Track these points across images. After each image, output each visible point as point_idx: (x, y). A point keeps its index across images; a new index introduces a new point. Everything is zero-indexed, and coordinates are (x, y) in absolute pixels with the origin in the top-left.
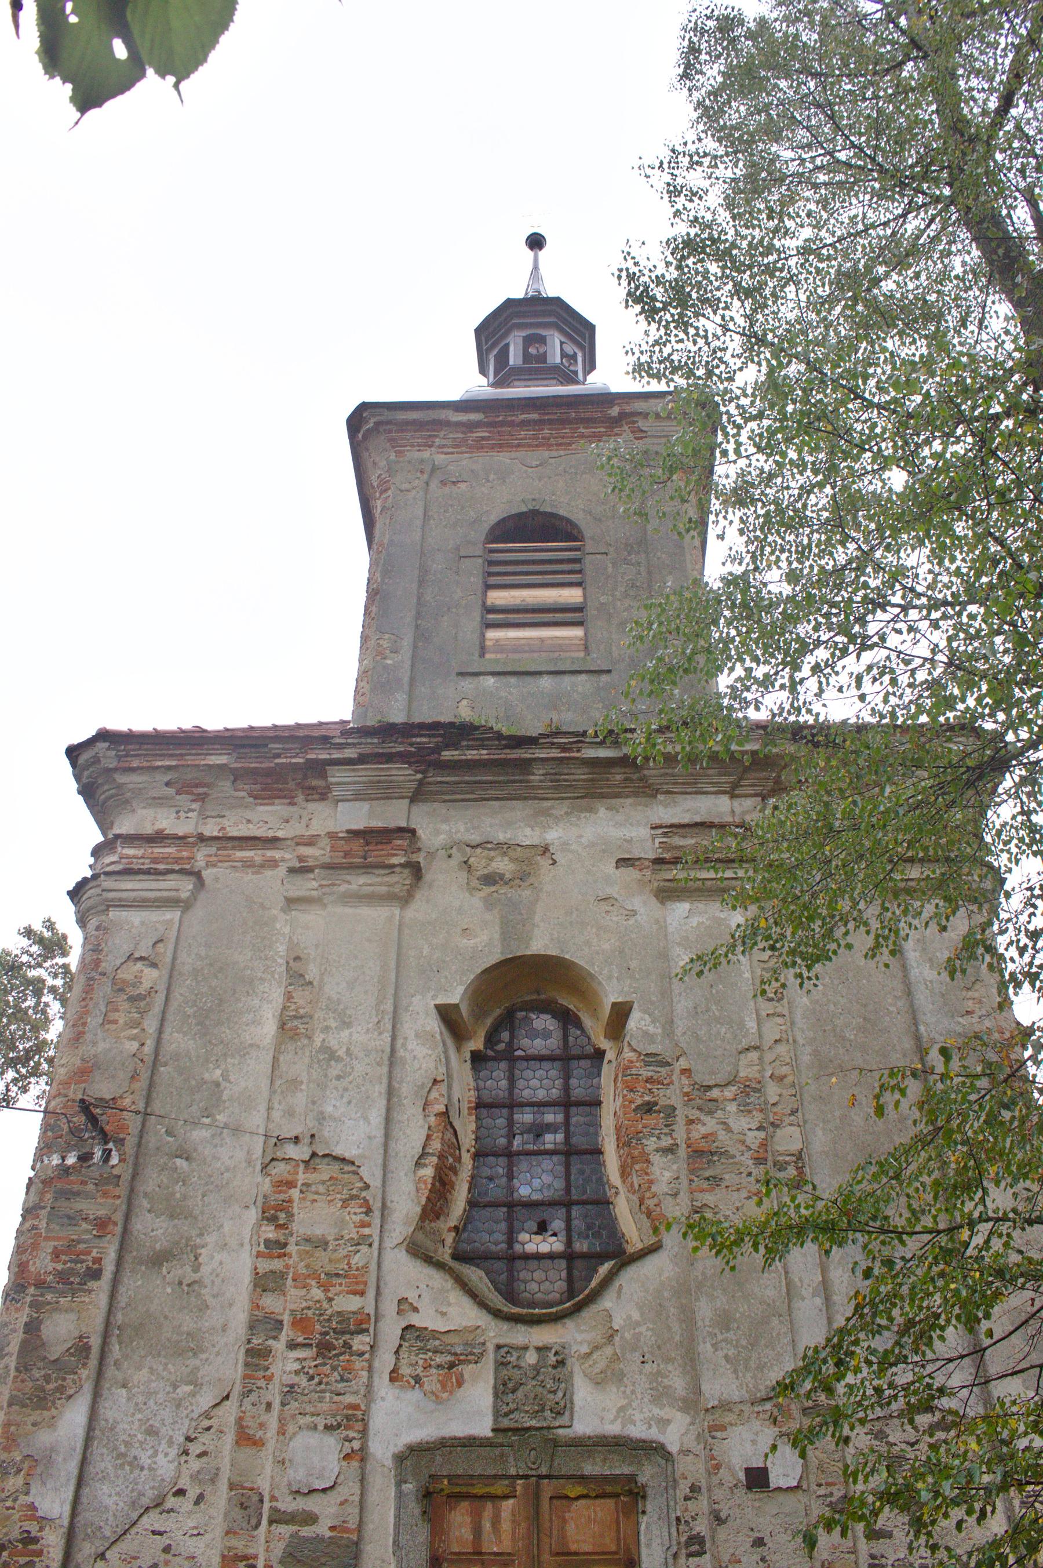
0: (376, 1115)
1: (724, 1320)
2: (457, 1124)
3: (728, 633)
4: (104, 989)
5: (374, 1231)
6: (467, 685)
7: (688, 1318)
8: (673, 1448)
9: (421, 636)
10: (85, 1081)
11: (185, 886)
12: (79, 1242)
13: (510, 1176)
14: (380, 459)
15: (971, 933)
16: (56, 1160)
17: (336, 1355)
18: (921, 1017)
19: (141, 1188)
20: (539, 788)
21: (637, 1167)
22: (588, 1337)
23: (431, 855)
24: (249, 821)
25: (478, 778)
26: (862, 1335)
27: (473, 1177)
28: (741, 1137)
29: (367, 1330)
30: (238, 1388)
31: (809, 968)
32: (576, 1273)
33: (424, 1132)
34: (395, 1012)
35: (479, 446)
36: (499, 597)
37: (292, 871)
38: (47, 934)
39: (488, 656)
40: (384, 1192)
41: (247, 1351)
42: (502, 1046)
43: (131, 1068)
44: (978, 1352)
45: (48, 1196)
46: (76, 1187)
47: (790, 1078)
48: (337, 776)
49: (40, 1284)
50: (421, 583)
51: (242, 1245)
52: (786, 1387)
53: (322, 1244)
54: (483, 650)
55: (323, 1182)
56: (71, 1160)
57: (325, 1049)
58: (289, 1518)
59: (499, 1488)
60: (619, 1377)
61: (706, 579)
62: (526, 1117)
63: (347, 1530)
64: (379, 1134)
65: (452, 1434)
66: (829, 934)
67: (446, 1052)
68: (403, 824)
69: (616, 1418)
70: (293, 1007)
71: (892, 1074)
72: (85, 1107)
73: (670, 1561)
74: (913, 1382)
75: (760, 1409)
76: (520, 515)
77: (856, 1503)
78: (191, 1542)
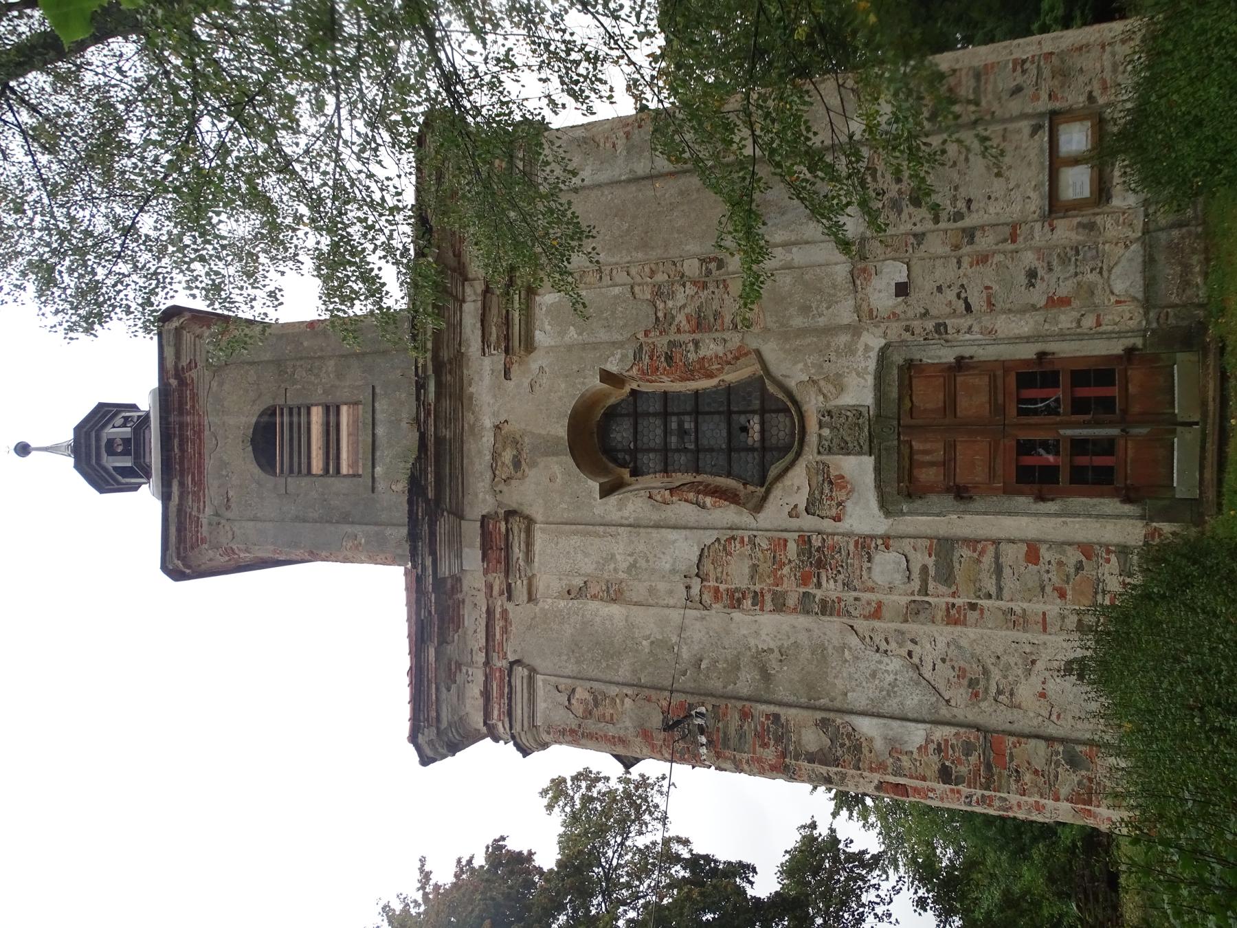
0: (672, 535)
1: (805, 309)
4: (591, 726)
5: (746, 534)
6: (381, 486)
7: (802, 332)
8: (883, 342)
9: (346, 519)
11: (520, 672)
12: (756, 730)
14: (207, 555)
16: (703, 750)
18: (616, 178)
20: (455, 432)
21: (707, 365)
24: (475, 632)
30: (845, 620)
32: (773, 408)
33: (683, 503)
35: (199, 484)
36: (317, 465)
38: (550, 794)
40: (722, 529)
41: (822, 614)
42: (627, 457)
43: (642, 702)
46: (721, 735)
47: (652, 266)
48: (444, 570)
50: (305, 521)
53: (754, 567)
55: (715, 568)
56: (703, 740)
59: (906, 451)
60: (839, 376)
63: (931, 546)
64: (684, 532)
67: (631, 491)
68: (478, 524)
73: (949, 344)
76: (254, 450)
78: (939, 645)
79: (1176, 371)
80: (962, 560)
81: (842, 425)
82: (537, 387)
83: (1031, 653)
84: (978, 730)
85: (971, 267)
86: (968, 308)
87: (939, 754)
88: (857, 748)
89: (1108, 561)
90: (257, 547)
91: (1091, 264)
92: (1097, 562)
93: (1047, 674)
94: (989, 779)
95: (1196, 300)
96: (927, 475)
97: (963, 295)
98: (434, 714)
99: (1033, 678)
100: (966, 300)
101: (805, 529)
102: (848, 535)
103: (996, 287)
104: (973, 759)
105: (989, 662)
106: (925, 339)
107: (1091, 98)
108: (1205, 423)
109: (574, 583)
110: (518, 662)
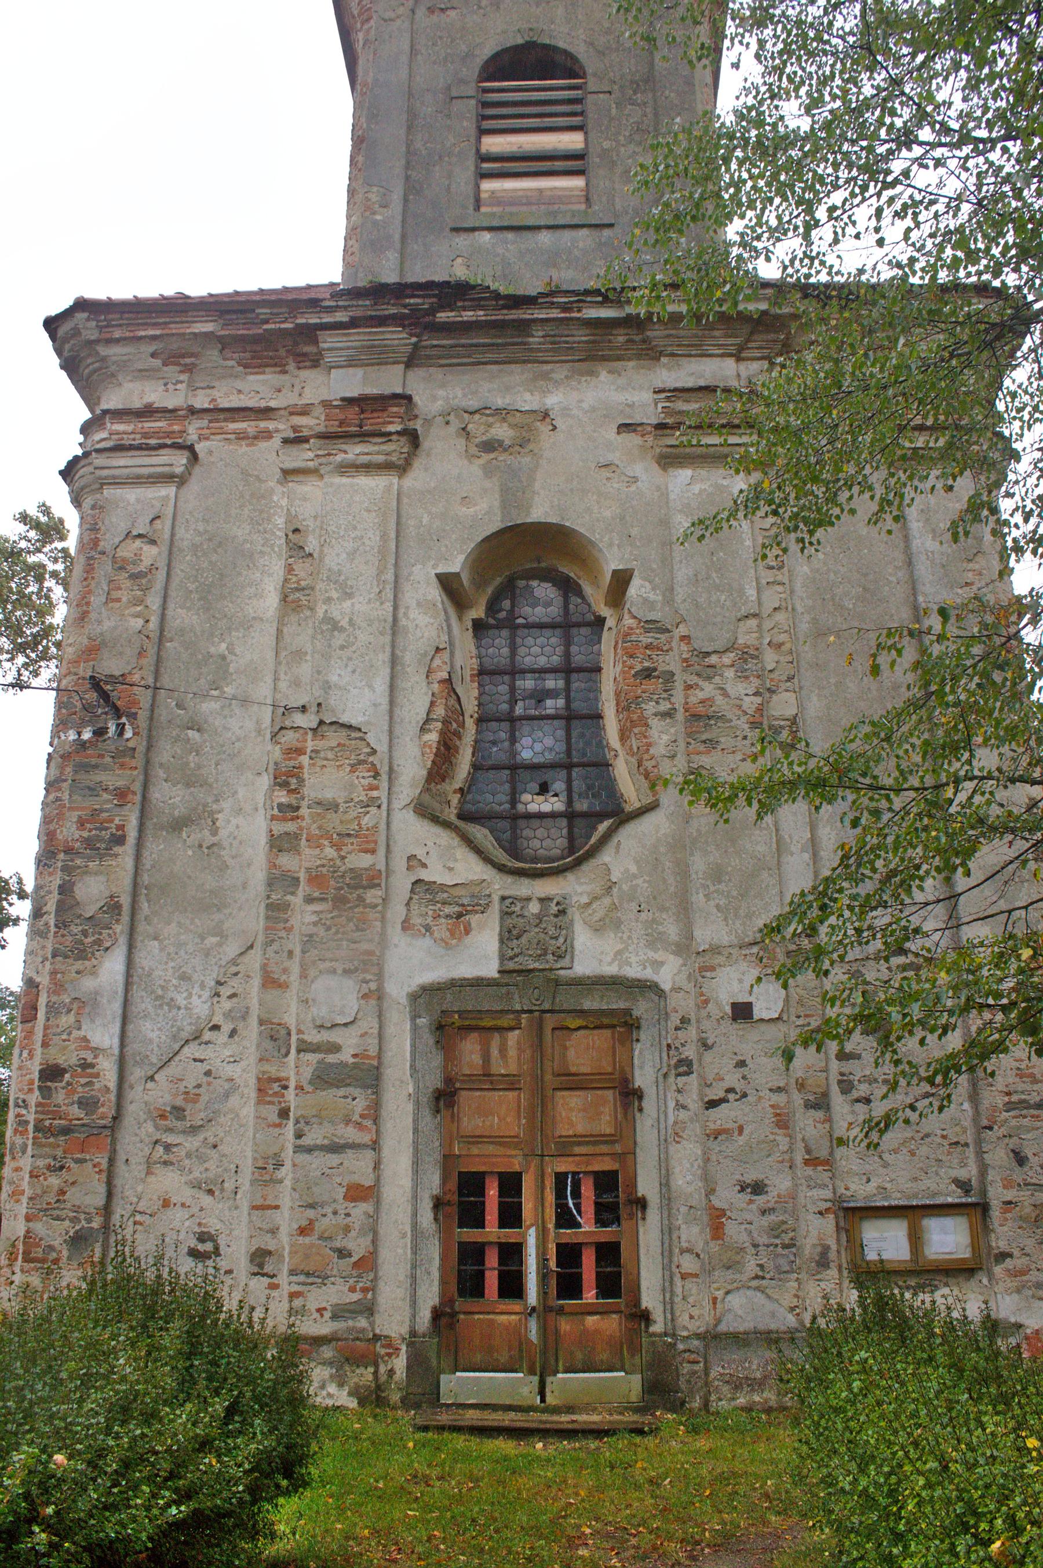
0: (381, 684)
1: (717, 874)
2: (459, 690)
3: (740, 176)
4: (104, 569)
5: (382, 794)
6: (462, 241)
7: (683, 872)
8: (666, 986)
9: (412, 189)
10: (94, 659)
11: (179, 461)
12: (102, 811)
13: (513, 740)
15: (978, 495)
16: (72, 736)
17: (350, 908)
18: (920, 587)
19: (156, 760)
20: (539, 350)
21: (636, 730)
22: (587, 888)
23: (428, 422)
24: (240, 392)
25: (475, 341)
26: (845, 884)
27: (476, 741)
28: (738, 702)
29: (379, 885)
30: (261, 938)
31: (811, 533)
33: (428, 699)
34: (396, 582)
36: (494, 144)
37: (286, 441)
38: (44, 519)
39: (483, 210)
40: (391, 758)
42: (503, 615)
44: (954, 897)
45: (68, 770)
46: (94, 761)
47: (788, 646)
48: (329, 341)
49: (69, 851)
50: (409, 128)
51: (256, 809)
52: (774, 929)
54: (478, 203)
55: (332, 749)
56: (87, 735)
57: (328, 619)
58: (315, 1048)
60: (617, 924)
61: (718, 111)
62: (528, 683)
63: (368, 1057)
64: (385, 701)
65: (461, 976)
66: (832, 499)
67: (447, 620)
69: (613, 961)
70: (294, 579)
71: (889, 634)
72: (95, 683)
73: (661, 1079)
74: (890, 924)
75: (748, 952)
76: (516, 48)
77: (833, 1024)
79: (615, 1374)
80: (349, 1100)
81: (545, 931)
82: (605, 473)
83: (222, 1190)
84: (115, 1118)
85: (772, 1106)
86: (712, 1104)
87: (79, 1066)
88: (81, 953)
89: (352, 1290)
90: (371, 57)
91: (770, 1265)
92: (351, 1276)
93: (195, 1210)
94: (49, 1131)
95: (713, 1397)
96: (470, 1052)
97: (731, 1097)
98: (117, 334)
99: (188, 1192)
100: (723, 1100)
101: (391, 879)
102: (383, 941)
103: (741, 1140)
104: (75, 1111)
105: (209, 1134)
106: (669, 1046)
107: (1003, 1256)
108: (544, 1411)
109: (311, 538)
110: (194, 457)
